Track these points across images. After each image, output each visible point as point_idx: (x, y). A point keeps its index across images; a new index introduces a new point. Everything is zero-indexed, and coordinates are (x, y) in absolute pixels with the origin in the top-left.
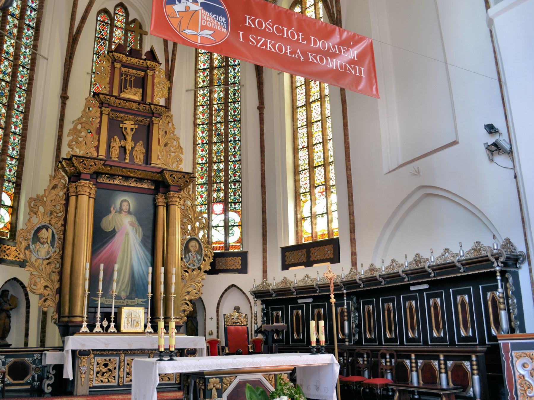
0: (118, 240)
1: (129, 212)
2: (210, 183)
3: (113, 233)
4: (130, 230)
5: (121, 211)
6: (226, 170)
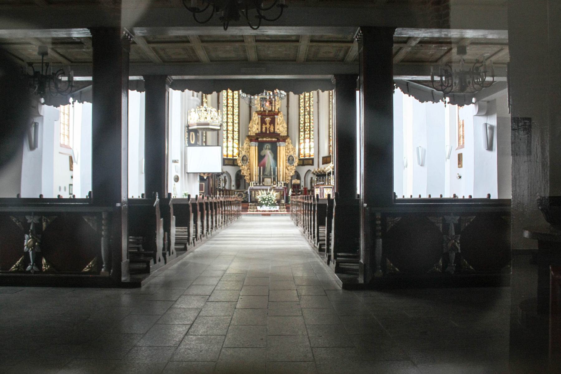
0: (266, 158)
1: (269, 149)
2: (305, 131)
3: (264, 156)
4: (269, 154)
5: (266, 149)
6: (310, 126)
